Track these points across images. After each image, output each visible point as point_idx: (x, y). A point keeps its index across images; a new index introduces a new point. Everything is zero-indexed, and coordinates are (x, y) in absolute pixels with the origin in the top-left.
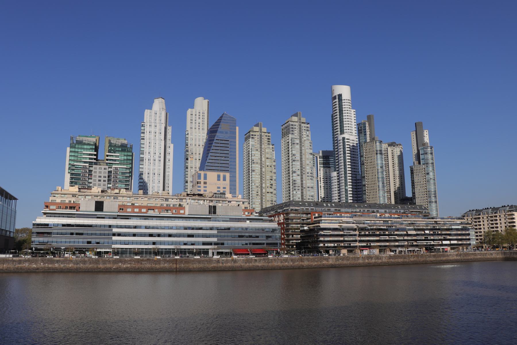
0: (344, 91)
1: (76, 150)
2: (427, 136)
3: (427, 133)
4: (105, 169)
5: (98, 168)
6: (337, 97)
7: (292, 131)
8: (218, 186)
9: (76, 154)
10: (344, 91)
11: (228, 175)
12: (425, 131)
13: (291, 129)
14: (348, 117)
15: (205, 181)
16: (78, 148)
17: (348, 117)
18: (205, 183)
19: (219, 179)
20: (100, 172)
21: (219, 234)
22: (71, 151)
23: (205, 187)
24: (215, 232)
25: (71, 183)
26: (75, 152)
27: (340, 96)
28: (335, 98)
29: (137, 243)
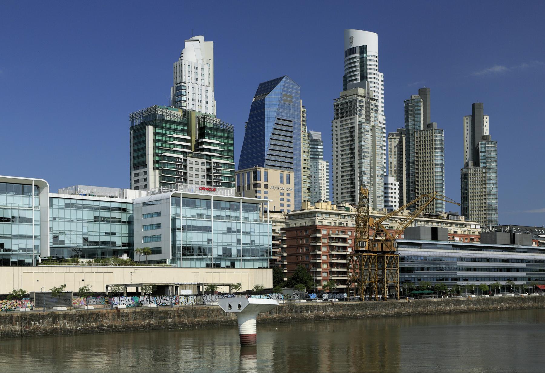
0: (369, 40)
1: (164, 132)
2: (488, 125)
3: (488, 120)
4: (203, 164)
5: (194, 163)
6: (358, 50)
7: (360, 110)
8: (281, 191)
9: (164, 139)
10: (369, 40)
11: (292, 175)
12: (485, 117)
13: (358, 108)
14: (375, 81)
15: (266, 183)
16: (166, 129)
17: (375, 81)
18: (266, 186)
19: (282, 182)
20: (197, 169)
21: (529, 268)
22: (155, 134)
23: (266, 193)
24: (524, 265)
25: (162, 184)
26: (161, 134)
27: (363, 49)
28: (353, 50)
29: (478, 279)
